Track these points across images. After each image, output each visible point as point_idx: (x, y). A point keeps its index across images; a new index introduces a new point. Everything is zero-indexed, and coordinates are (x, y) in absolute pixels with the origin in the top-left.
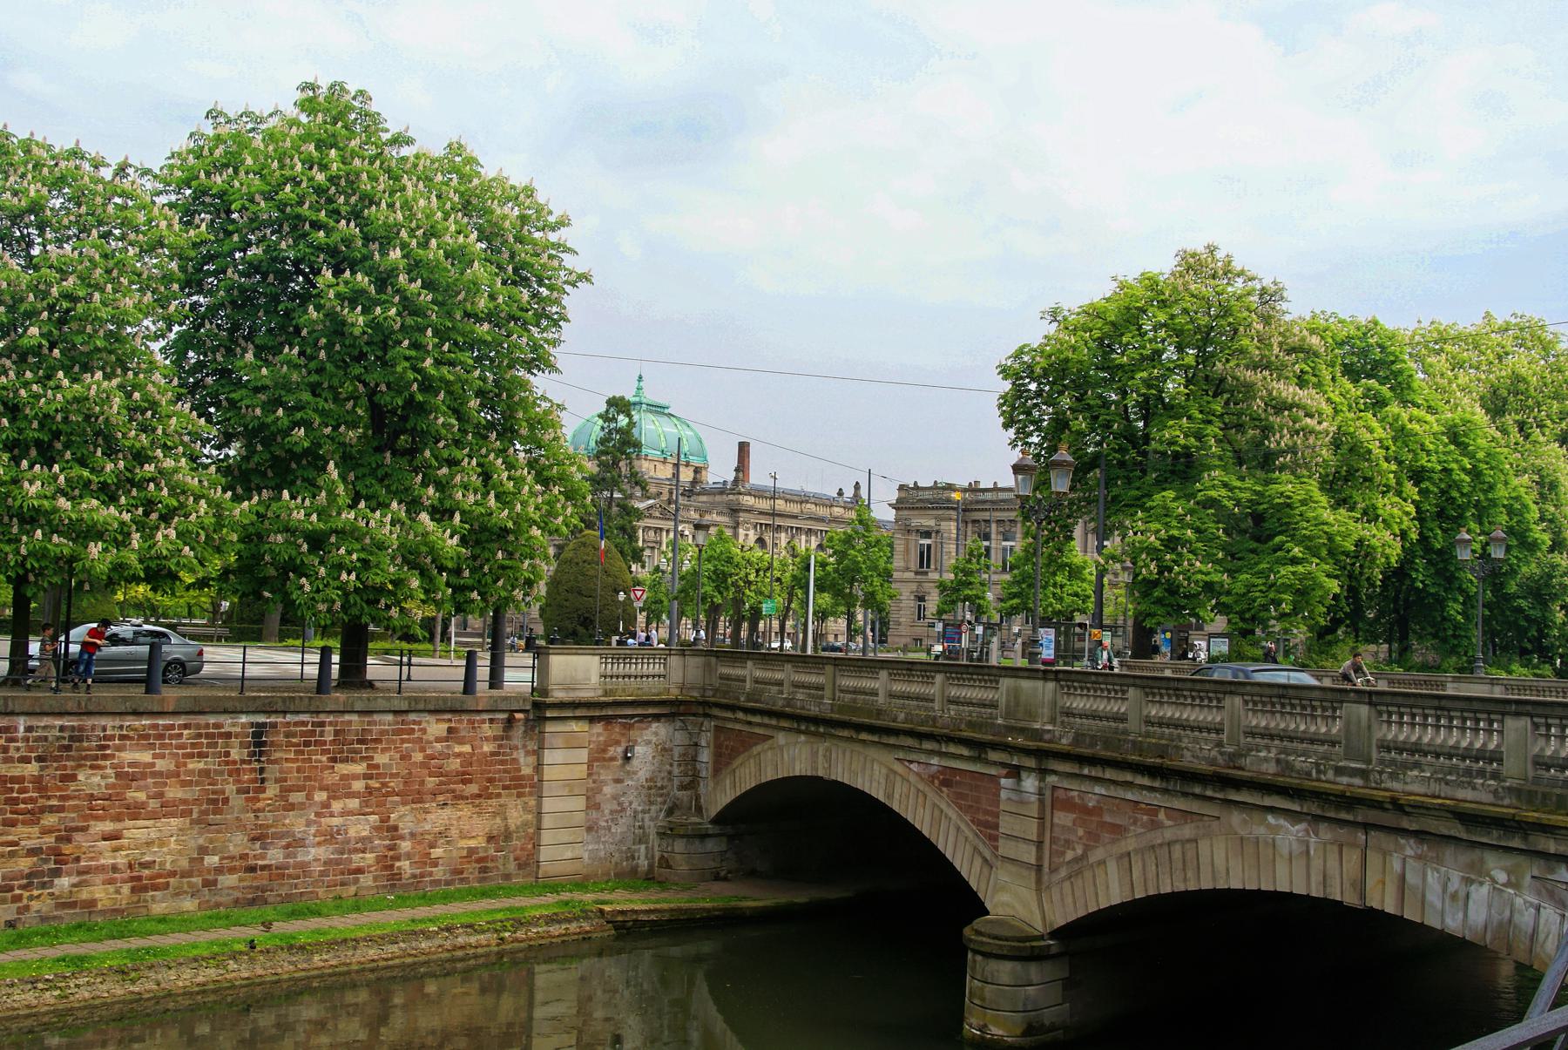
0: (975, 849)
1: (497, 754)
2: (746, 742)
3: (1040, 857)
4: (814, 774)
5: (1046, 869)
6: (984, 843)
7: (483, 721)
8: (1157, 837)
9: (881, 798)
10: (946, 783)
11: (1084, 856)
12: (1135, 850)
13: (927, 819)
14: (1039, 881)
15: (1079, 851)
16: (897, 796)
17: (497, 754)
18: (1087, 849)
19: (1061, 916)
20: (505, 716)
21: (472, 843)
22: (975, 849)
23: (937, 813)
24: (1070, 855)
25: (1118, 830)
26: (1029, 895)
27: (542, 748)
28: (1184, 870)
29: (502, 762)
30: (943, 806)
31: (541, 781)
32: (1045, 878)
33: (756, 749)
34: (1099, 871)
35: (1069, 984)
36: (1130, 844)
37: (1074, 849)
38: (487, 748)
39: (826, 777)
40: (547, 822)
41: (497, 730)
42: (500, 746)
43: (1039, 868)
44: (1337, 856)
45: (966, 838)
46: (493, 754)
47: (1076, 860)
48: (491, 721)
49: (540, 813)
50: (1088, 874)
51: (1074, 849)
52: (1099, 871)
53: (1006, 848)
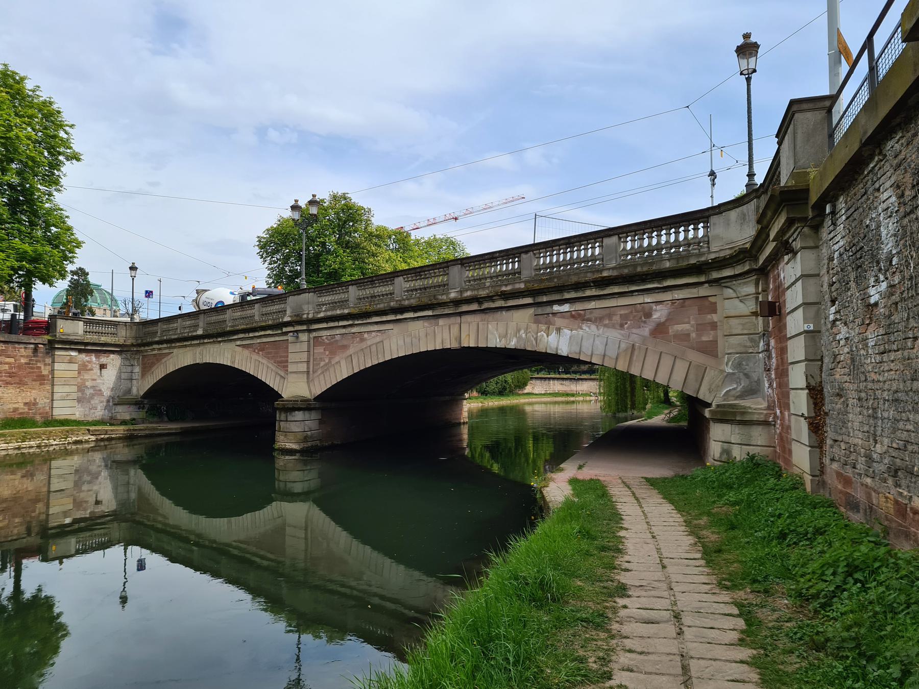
0: (277, 373)
1: (29, 364)
2: (159, 358)
3: (308, 368)
4: (195, 363)
5: (311, 372)
6: (281, 370)
7: (21, 348)
8: (364, 345)
9: (229, 364)
10: (262, 350)
11: (330, 362)
12: (354, 353)
13: (252, 366)
14: (308, 378)
15: (327, 361)
16: (237, 361)
17: (29, 364)
18: (330, 359)
19: (318, 391)
20: (32, 346)
21: (16, 406)
22: (277, 373)
23: (257, 363)
24: (322, 364)
25: (345, 347)
26: (305, 386)
27: (53, 362)
28: (377, 355)
29: (32, 368)
30: (260, 360)
31: (53, 378)
32: (311, 376)
33: (163, 360)
34: (337, 367)
35: (321, 422)
36: (351, 351)
37: (324, 361)
38: (23, 361)
39: (201, 362)
40: (56, 396)
41: (29, 352)
42: (30, 360)
43: (308, 372)
44: (448, 330)
45: (272, 370)
46: (26, 363)
47: (326, 365)
48: (25, 348)
49: (53, 393)
50: (332, 370)
51: (324, 361)
52: (337, 367)
53: (291, 368)
